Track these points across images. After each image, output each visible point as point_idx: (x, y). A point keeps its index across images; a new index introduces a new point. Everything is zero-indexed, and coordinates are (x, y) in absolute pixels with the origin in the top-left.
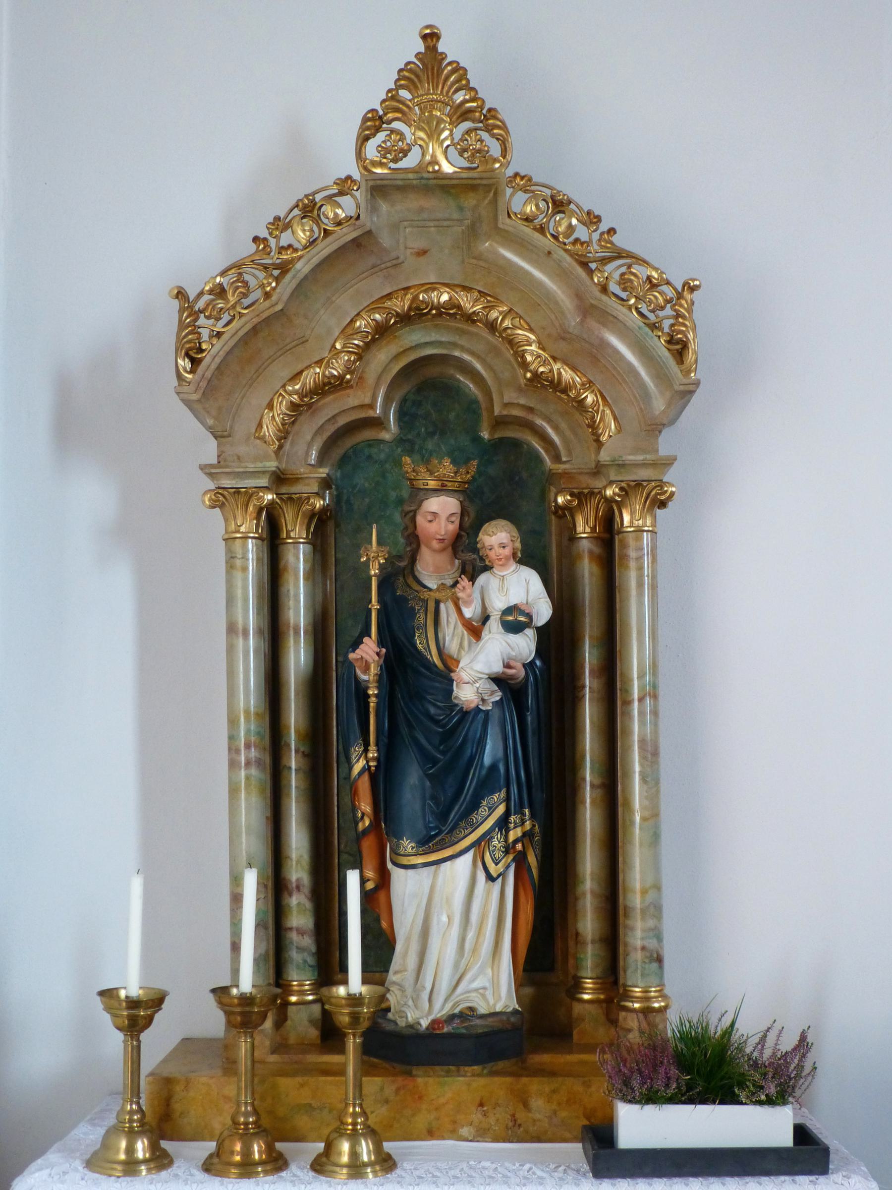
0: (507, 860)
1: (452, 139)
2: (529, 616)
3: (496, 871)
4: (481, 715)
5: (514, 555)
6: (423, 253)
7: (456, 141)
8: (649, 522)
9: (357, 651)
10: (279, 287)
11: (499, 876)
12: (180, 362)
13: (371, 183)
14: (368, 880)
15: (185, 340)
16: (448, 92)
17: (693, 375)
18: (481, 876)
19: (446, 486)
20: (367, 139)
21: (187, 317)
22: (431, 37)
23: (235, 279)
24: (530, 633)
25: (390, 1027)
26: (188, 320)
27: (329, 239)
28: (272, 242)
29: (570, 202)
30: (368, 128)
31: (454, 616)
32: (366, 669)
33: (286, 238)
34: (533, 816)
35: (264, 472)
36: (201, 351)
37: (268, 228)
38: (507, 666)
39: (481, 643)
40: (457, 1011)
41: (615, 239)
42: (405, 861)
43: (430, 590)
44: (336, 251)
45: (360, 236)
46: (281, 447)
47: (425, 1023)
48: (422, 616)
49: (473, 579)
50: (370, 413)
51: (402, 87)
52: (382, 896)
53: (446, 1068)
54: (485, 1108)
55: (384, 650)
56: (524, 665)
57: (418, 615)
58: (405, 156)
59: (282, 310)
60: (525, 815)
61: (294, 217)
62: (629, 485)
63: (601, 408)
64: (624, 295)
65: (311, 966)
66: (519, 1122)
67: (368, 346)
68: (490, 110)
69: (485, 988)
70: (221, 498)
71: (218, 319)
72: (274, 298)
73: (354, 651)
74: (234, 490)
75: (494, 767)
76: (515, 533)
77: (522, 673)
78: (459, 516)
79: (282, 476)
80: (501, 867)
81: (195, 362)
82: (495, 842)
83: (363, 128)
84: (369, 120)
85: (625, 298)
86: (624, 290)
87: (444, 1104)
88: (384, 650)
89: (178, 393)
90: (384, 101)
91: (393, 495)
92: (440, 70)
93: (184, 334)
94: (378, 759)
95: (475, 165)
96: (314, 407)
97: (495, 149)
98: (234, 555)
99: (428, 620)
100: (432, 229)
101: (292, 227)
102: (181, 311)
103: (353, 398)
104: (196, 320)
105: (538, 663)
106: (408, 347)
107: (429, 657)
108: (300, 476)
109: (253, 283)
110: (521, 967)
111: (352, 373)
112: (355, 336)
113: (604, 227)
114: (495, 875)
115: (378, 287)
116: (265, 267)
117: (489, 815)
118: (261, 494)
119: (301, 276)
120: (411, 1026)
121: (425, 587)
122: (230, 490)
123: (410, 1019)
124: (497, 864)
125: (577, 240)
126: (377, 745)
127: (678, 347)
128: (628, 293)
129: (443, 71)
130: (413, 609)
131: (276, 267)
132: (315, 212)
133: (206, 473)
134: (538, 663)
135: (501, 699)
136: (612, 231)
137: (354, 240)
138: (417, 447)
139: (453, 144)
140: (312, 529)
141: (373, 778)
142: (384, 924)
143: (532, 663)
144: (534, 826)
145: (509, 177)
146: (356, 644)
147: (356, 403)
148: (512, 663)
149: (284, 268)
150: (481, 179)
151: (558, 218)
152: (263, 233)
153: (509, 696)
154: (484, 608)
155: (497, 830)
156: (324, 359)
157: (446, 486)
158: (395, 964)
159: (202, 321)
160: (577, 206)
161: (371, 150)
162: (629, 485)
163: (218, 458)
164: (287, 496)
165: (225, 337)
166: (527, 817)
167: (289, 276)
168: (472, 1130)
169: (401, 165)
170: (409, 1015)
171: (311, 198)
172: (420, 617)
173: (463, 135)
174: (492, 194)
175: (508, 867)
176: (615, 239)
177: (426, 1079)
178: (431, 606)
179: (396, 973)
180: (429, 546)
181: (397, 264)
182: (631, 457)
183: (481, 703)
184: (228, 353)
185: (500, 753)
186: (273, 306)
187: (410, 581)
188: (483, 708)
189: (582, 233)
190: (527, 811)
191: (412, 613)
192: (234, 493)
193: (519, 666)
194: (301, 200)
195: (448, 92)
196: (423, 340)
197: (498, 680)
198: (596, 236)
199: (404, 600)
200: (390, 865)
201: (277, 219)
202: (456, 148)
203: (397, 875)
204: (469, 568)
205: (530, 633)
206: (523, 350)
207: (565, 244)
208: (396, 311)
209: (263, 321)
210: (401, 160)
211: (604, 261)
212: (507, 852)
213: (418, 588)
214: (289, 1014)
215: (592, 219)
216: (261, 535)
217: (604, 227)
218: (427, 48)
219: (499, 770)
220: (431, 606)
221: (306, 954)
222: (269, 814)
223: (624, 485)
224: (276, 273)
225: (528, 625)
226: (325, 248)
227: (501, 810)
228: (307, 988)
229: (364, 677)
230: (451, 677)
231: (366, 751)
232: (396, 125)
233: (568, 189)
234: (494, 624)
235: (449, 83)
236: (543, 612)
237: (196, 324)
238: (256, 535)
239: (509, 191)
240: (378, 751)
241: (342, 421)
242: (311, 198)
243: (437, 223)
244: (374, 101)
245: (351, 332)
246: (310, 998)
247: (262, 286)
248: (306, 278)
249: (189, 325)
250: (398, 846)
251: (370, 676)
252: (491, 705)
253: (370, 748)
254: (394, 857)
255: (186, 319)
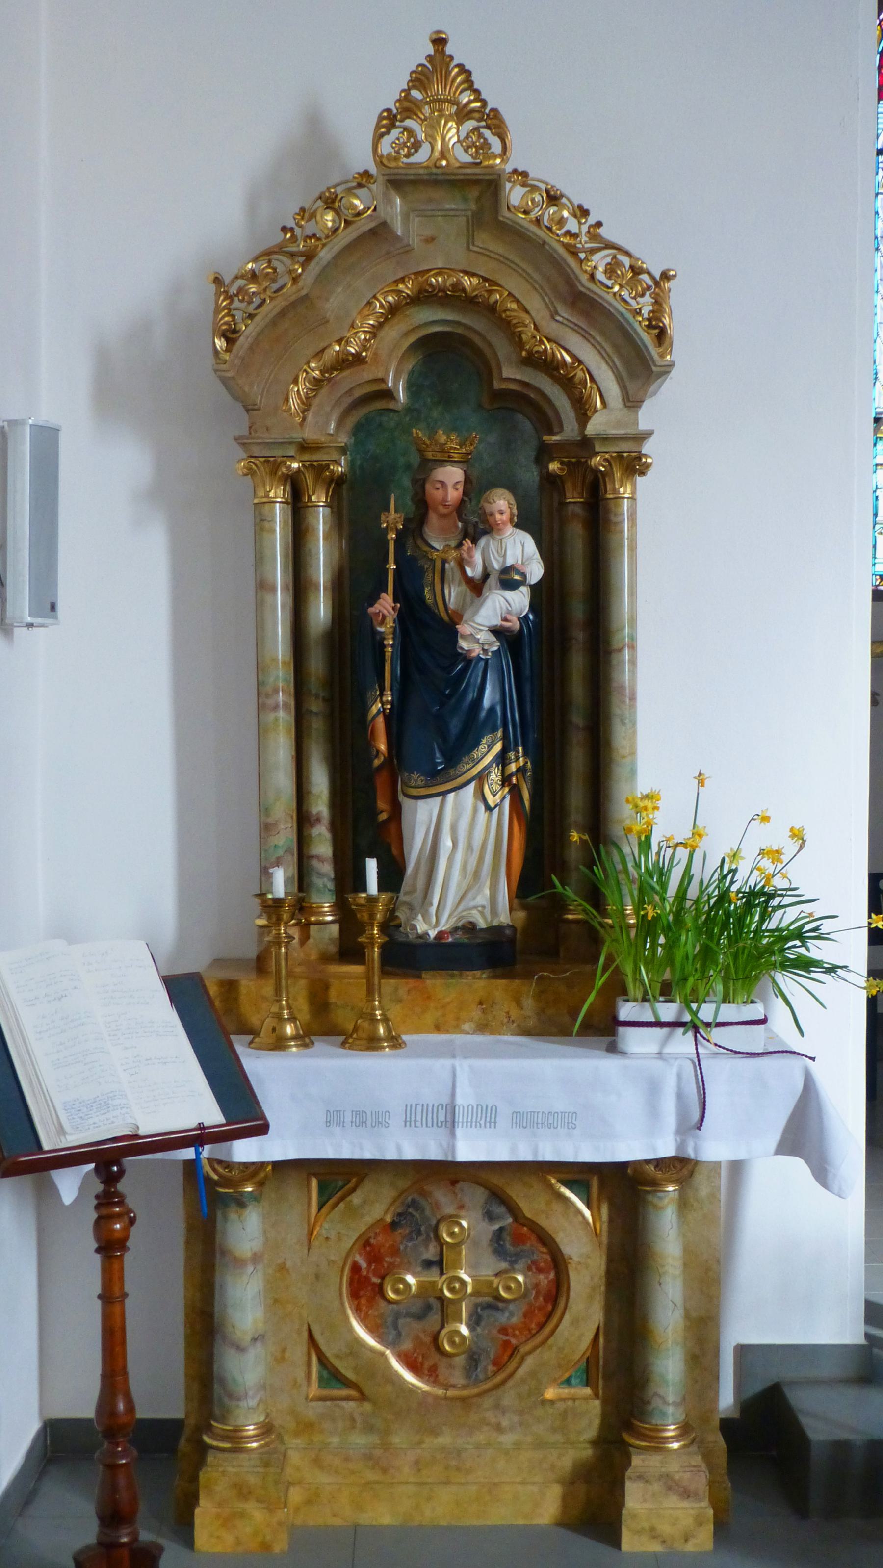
0: (503, 792)
1: (459, 137)
2: (524, 575)
3: (494, 801)
4: (482, 664)
5: (511, 520)
6: (431, 240)
7: (462, 138)
8: (629, 490)
9: (376, 605)
10: (304, 274)
11: (496, 806)
12: (217, 341)
13: (386, 177)
14: (382, 812)
15: (222, 322)
16: (455, 94)
17: (668, 357)
18: (482, 807)
19: (453, 457)
20: (382, 135)
21: (223, 301)
22: (439, 42)
23: (265, 265)
24: (525, 590)
25: (401, 939)
26: (224, 303)
27: (350, 229)
28: (298, 231)
29: (562, 196)
30: (383, 126)
31: (458, 574)
32: (383, 622)
33: (310, 228)
34: (525, 754)
35: (290, 443)
36: (235, 331)
37: (295, 219)
38: (505, 620)
39: (482, 598)
40: (460, 924)
41: (601, 231)
42: (414, 792)
43: (438, 551)
44: (355, 240)
45: (376, 226)
46: (304, 419)
47: (433, 934)
48: (431, 575)
49: (475, 541)
50: (382, 387)
51: (415, 87)
52: (393, 827)
53: (451, 972)
54: (484, 1006)
55: (399, 605)
56: (519, 619)
57: (427, 574)
58: (416, 151)
59: (307, 294)
60: (518, 753)
61: (318, 208)
62: (611, 456)
63: (589, 385)
64: (609, 283)
65: (330, 890)
66: (512, 1018)
67: (381, 325)
68: (492, 110)
69: (483, 907)
70: (254, 467)
71: (250, 302)
72: (301, 284)
73: (372, 605)
74: (264, 459)
75: (492, 709)
76: (513, 501)
77: (517, 626)
78: (462, 483)
79: (305, 445)
80: (498, 798)
81: (230, 342)
82: (493, 776)
83: (378, 126)
84: (384, 118)
85: (610, 285)
86: (610, 278)
87: (449, 1003)
88: (399, 605)
89: (216, 371)
90: (399, 100)
91: (402, 461)
92: (448, 73)
93: (220, 316)
94: (392, 703)
95: (478, 161)
96: (333, 381)
97: (496, 145)
98: (264, 518)
99: (436, 578)
100: (440, 218)
101: (315, 217)
102: (218, 295)
103: (367, 374)
104: (232, 301)
105: (531, 617)
106: (417, 325)
107: (436, 611)
108: (321, 445)
109: (280, 269)
110: (515, 885)
111: (366, 350)
112: (370, 317)
113: (592, 220)
114: (492, 806)
115: (390, 271)
116: (292, 255)
117: (488, 752)
118: (289, 463)
119: (324, 262)
120: (420, 937)
121: (433, 548)
122: (261, 459)
123: (419, 931)
124: (494, 796)
125: (568, 233)
126: (391, 690)
127: (657, 331)
128: (613, 281)
129: (450, 72)
130: (422, 567)
131: (302, 254)
132: (337, 204)
133: (238, 443)
134: (531, 617)
135: (499, 649)
136: (599, 224)
137: (371, 230)
138: (423, 416)
139: (459, 141)
140: (330, 494)
141: (388, 719)
142: (395, 851)
143: (526, 616)
144: (527, 763)
145: (509, 173)
146: (373, 598)
147: (371, 377)
148: (509, 617)
149: (309, 256)
150: (484, 174)
151: (551, 212)
152: (291, 223)
153: (506, 646)
154: (485, 568)
155: (494, 765)
156: (344, 338)
157: (453, 457)
158: (406, 886)
159: (236, 303)
160: (568, 199)
161: (386, 147)
162: (611, 456)
163: (249, 430)
164: (308, 463)
165: (257, 319)
166: (521, 754)
167: (313, 264)
168: (473, 1025)
169: (412, 160)
170: (418, 927)
171: (332, 190)
172: (428, 577)
173: (468, 134)
174: (493, 187)
175: (504, 798)
176: (601, 231)
177: (433, 981)
178: (438, 564)
179: (406, 893)
180: (436, 510)
181: (408, 250)
182: (614, 432)
183: (482, 652)
184: (259, 334)
185: (498, 697)
186: (299, 290)
187: (420, 542)
188: (483, 657)
189: (572, 225)
190: (520, 749)
191: (422, 572)
192: (265, 461)
193: (514, 619)
194: (324, 193)
195: (455, 94)
196: (431, 319)
197: (496, 632)
198: (585, 228)
199: (414, 559)
200: (401, 797)
201: (303, 210)
202: (462, 145)
203: (407, 804)
204: (471, 530)
205: (525, 590)
206: (520, 331)
207: (558, 235)
208: (406, 293)
209: (290, 304)
210: (413, 155)
211: (593, 251)
212: (503, 785)
213: (426, 549)
214: (311, 933)
215: (582, 212)
216: (287, 500)
217: (592, 220)
218: (436, 51)
219: (496, 712)
220: (438, 564)
221: (325, 880)
222: (294, 753)
223: (607, 456)
224: (302, 259)
225: (523, 582)
226: (345, 237)
227: (498, 747)
228: (326, 909)
229: (381, 629)
230: (456, 629)
231: (382, 695)
232: (409, 123)
233: (561, 185)
234: (493, 580)
235: (456, 85)
236: (536, 571)
237: (231, 307)
238: (283, 500)
239: (508, 186)
240: (392, 695)
241: (358, 393)
242: (332, 190)
243: (443, 213)
244: (389, 100)
245: (367, 313)
246: (329, 918)
247: (290, 272)
248: (328, 265)
249: (224, 308)
250: (409, 779)
251: (387, 628)
252: (490, 654)
253: (385, 693)
254: (405, 788)
255: (222, 303)
